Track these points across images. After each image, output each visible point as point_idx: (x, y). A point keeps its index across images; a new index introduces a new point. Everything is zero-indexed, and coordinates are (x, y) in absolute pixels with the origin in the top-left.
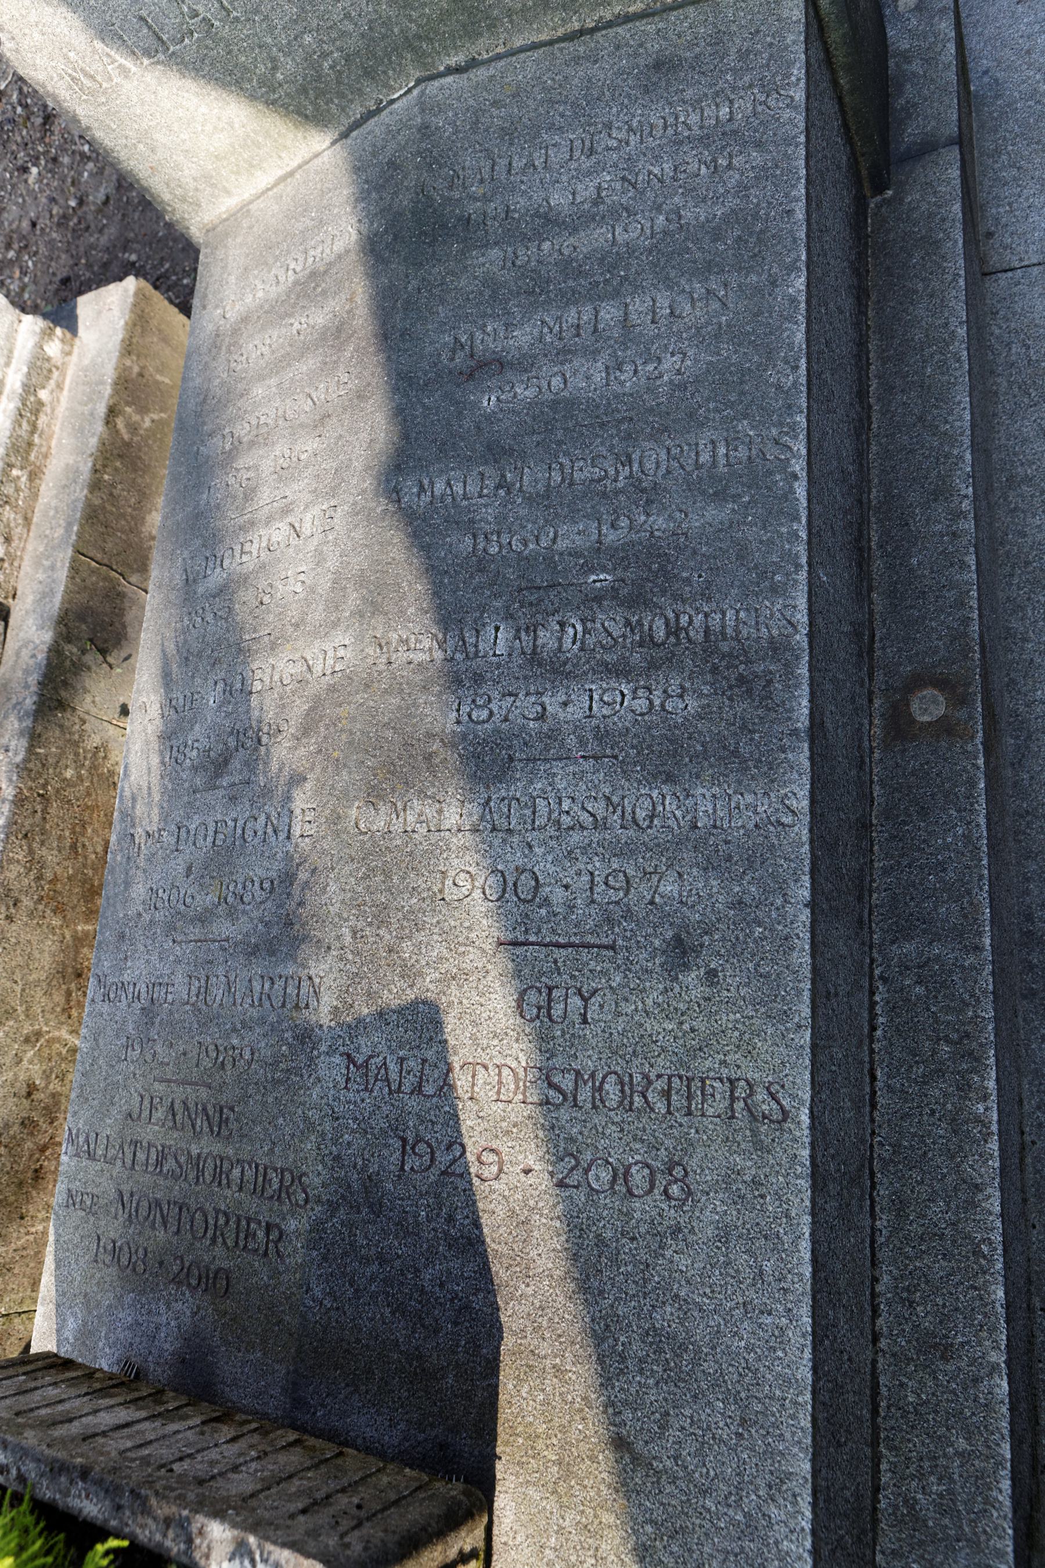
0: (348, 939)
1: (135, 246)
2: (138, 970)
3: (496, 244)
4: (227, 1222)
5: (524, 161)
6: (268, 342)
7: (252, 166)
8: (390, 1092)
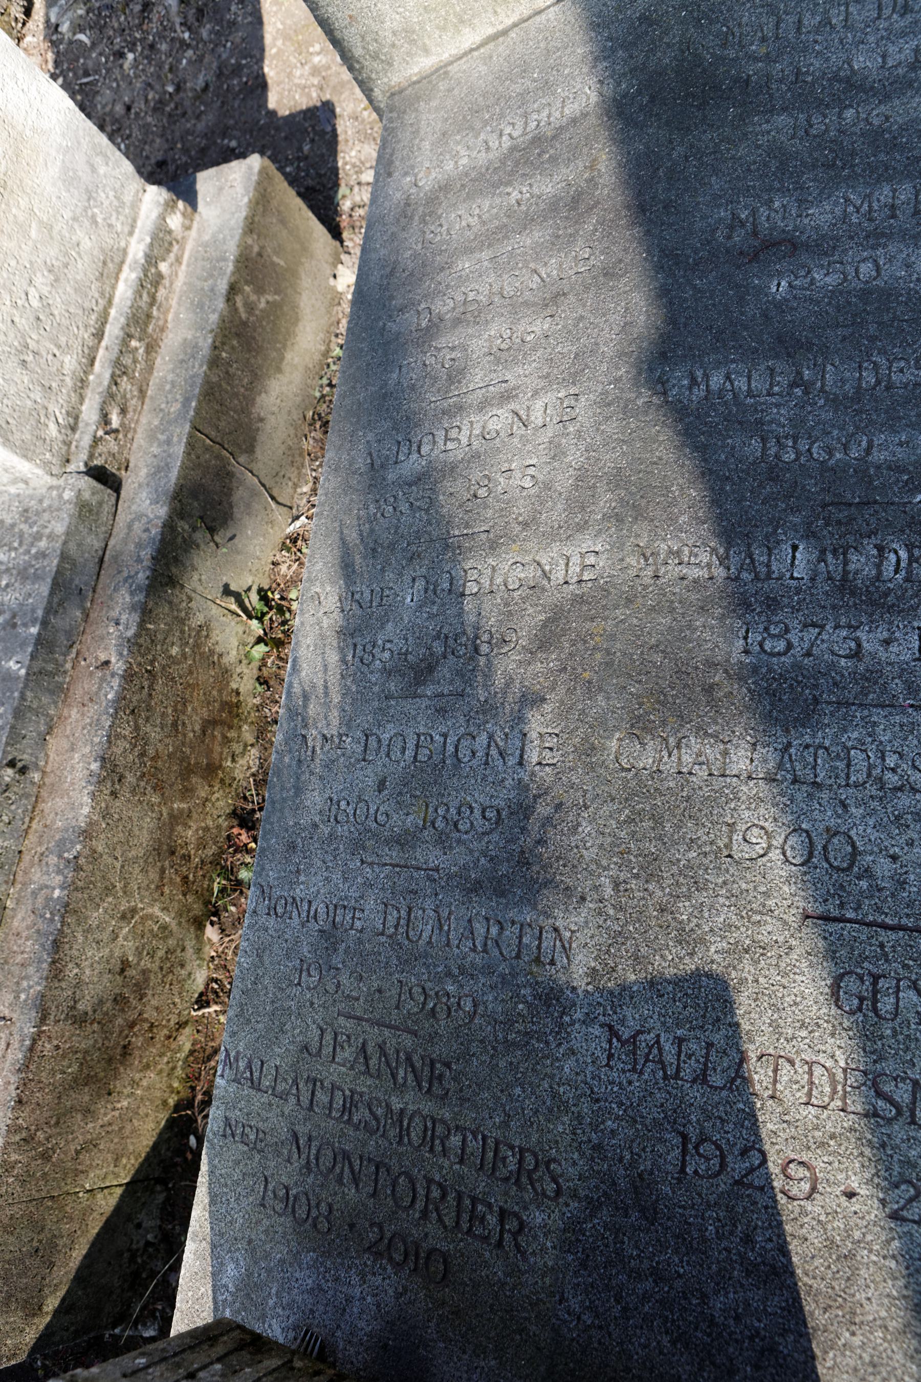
0: (609, 891)
1: (235, 132)
2: (316, 886)
3: (784, 109)
4: (444, 1196)
5: (818, 19)
6: (477, 211)
7: (462, 21)
8: (665, 1077)
